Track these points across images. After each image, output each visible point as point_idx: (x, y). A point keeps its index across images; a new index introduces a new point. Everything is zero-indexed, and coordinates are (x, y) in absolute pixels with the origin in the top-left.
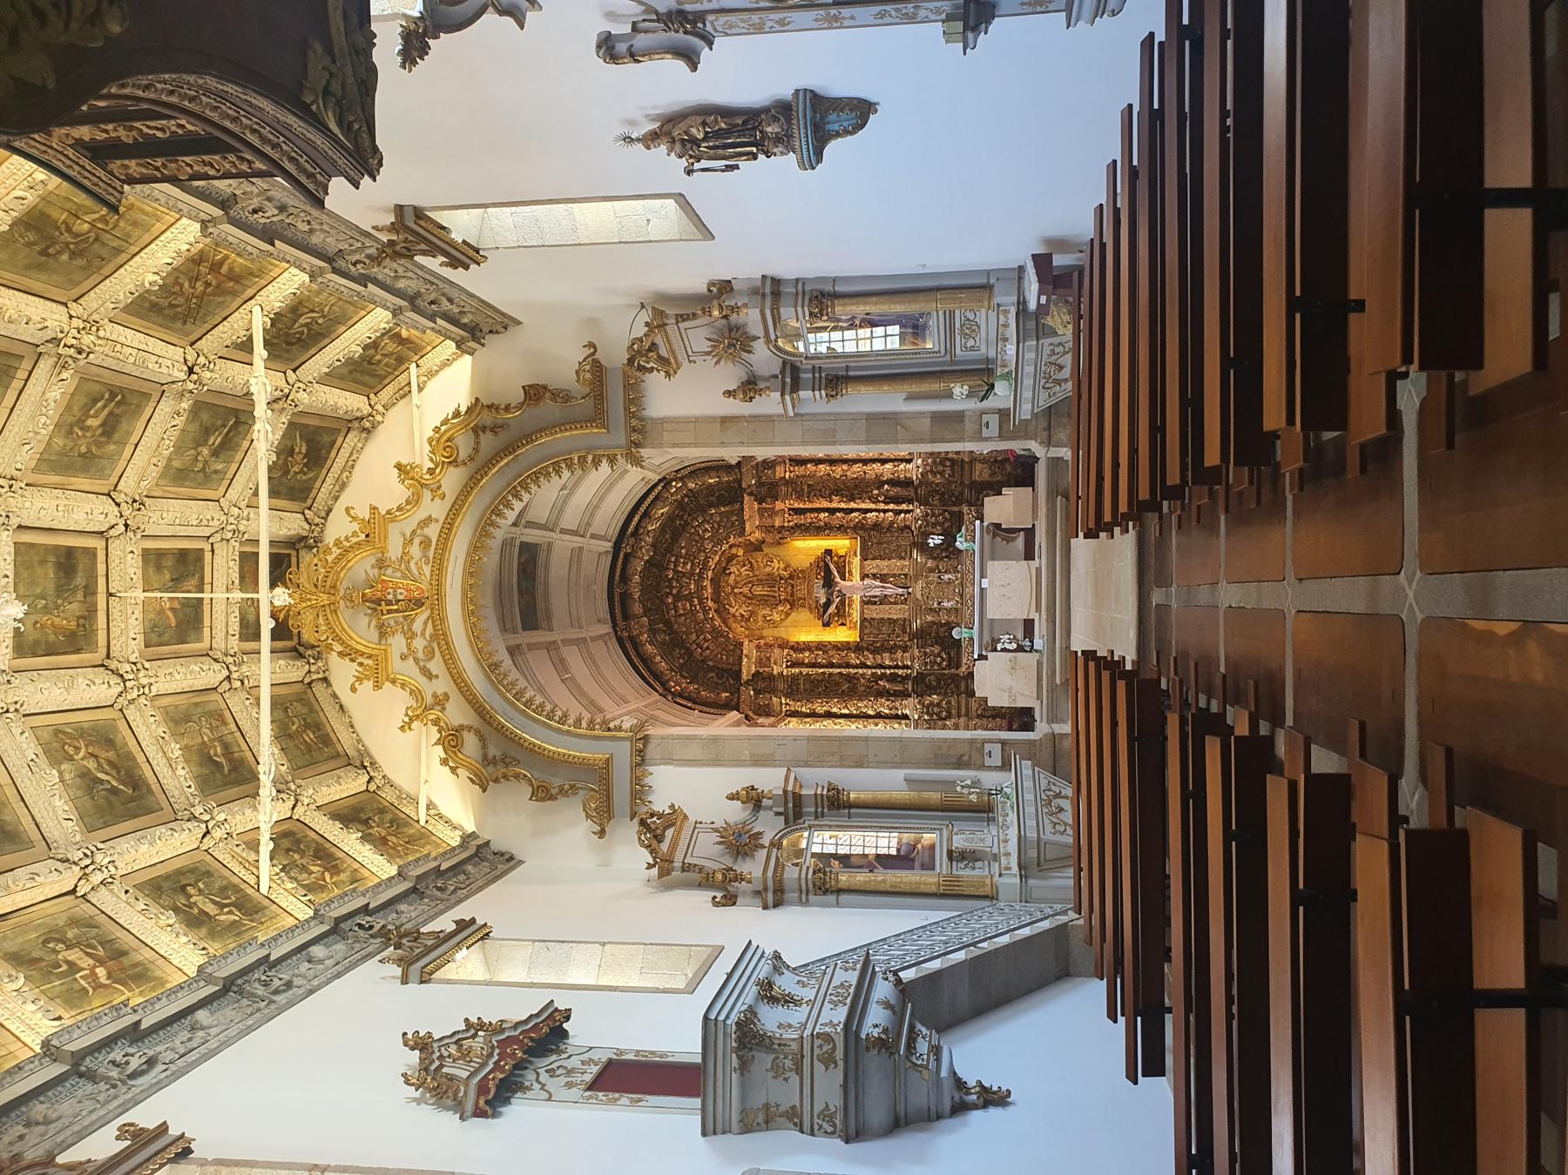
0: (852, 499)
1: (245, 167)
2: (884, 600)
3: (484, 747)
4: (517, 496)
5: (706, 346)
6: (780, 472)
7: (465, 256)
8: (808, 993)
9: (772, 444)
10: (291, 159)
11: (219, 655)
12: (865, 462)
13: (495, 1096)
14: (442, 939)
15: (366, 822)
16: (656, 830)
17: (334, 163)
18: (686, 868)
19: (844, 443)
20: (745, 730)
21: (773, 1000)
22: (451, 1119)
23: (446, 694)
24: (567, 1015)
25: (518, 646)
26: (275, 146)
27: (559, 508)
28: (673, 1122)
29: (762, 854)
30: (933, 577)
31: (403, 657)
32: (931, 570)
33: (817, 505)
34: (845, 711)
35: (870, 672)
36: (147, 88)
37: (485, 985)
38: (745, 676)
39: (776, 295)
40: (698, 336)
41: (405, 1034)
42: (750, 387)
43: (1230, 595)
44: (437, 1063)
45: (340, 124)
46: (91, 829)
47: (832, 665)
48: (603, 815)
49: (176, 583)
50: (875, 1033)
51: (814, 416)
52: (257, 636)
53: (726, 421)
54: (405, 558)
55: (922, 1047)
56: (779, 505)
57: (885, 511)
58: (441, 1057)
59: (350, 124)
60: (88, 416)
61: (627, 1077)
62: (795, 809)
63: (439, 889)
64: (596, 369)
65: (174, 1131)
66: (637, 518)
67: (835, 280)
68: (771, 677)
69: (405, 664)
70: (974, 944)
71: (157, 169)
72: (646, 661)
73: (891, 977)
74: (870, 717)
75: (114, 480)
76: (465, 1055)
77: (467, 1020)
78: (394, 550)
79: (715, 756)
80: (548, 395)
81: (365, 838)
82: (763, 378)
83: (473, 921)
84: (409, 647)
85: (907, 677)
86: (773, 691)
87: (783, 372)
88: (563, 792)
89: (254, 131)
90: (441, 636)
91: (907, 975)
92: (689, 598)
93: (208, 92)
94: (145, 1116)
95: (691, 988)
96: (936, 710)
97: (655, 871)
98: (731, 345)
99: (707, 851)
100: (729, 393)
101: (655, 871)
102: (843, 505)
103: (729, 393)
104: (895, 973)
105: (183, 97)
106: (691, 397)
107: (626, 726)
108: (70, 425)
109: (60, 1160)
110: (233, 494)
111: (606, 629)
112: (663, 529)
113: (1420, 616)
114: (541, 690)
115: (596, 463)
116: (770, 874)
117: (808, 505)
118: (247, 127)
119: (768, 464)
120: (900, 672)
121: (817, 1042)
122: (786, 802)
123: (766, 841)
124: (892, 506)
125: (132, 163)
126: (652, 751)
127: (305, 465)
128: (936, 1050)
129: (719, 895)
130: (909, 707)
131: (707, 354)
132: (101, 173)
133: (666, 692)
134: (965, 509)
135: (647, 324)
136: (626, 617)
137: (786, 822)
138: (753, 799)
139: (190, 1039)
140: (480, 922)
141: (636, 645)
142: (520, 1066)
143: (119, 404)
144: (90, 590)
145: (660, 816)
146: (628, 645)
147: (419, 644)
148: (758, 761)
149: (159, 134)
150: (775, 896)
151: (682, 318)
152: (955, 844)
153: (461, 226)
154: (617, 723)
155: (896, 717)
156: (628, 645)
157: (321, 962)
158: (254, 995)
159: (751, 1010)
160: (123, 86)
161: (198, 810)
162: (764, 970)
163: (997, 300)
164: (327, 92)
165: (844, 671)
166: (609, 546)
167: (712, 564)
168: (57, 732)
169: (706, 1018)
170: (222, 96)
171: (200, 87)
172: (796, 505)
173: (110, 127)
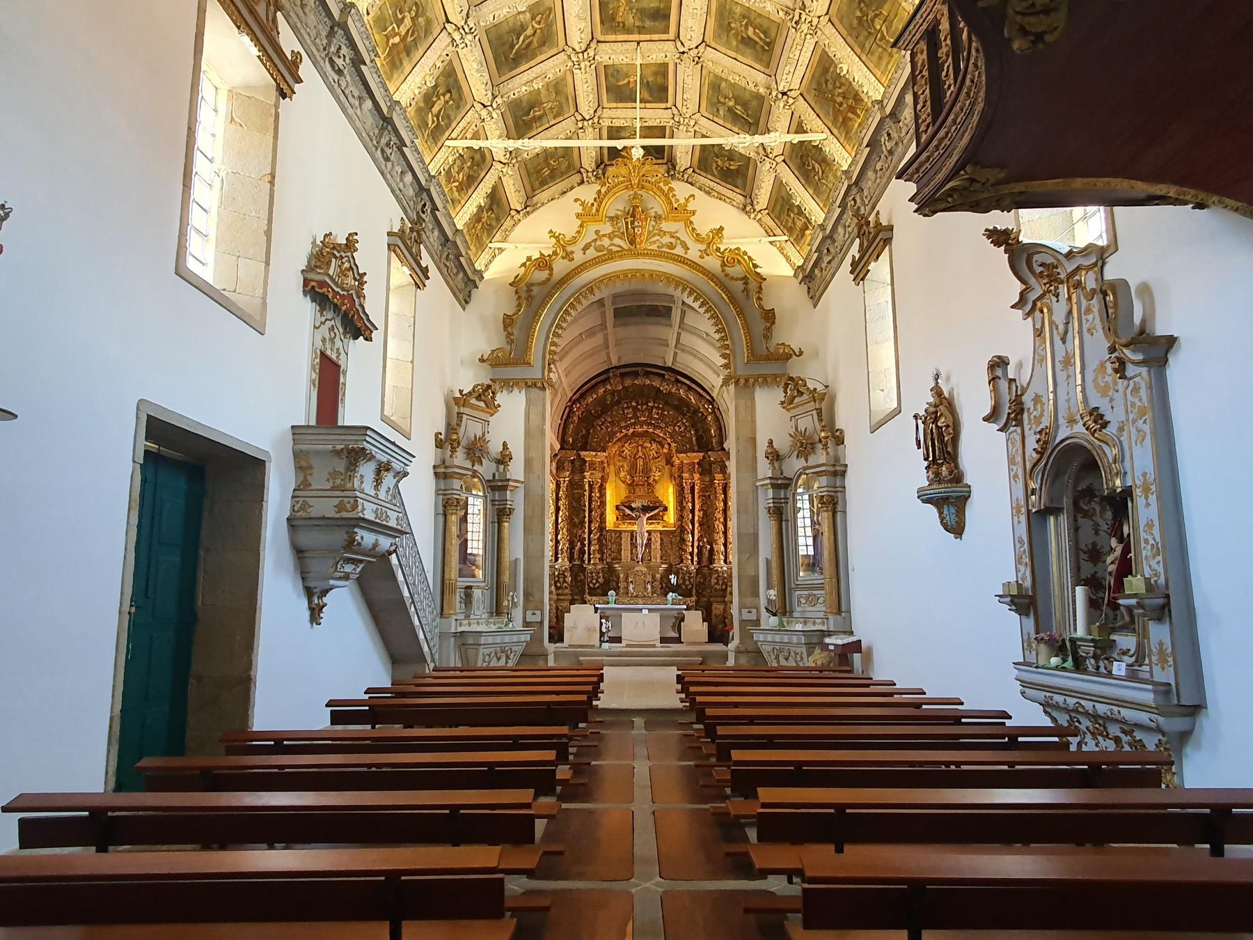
0: (701, 525)
1: (923, 128)
2: (634, 545)
5: (801, 427)
6: (719, 476)
7: (859, 271)
8: (382, 495)
9: (738, 471)
10: (928, 158)
12: (725, 533)
13: (317, 292)
15: (491, 209)
16: (484, 395)
26: (937, 147)
27: (694, 331)
30: (649, 578)
31: (597, 232)
32: (653, 577)
37: (387, 286)
38: (583, 453)
40: (808, 423)
42: (775, 456)
43: (642, 768)
45: (952, 189)
47: (590, 512)
48: (493, 361)
49: (646, 85)
50: (358, 538)
53: (753, 440)
54: (662, 233)
55: (348, 568)
56: (697, 476)
58: (342, 257)
59: (951, 196)
61: (329, 377)
64: (786, 356)
65: (297, 87)
67: (844, 512)
70: (413, 602)
73: (393, 548)
75: (713, 45)
79: (532, 435)
81: (480, 208)
83: (428, 278)
87: (785, 478)
89: (947, 134)
90: (611, 256)
91: (393, 558)
93: (973, 105)
94: (306, 69)
95: (384, 419)
99: (470, 429)
100: (771, 442)
103: (771, 442)
106: (769, 418)
107: (552, 375)
109: (279, 14)
110: (703, 121)
111: (615, 362)
112: (681, 399)
113: (633, 891)
115: (724, 356)
117: (696, 496)
119: (723, 469)
121: (352, 500)
125: (925, 56)
126: (535, 392)
128: (346, 577)
129: (442, 437)
130: (563, 562)
133: (573, 402)
134: (694, 599)
138: (504, 459)
140: (427, 282)
141: (603, 381)
142: (336, 308)
144: (641, 30)
145: (493, 398)
147: (606, 242)
148: (528, 463)
149: (944, 74)
150: (442, 473)
153: (879, 269)
157: (402, 180)
162: (397, 466)
164: (972, 181)
170: (970, 113)
173: (948, 42)
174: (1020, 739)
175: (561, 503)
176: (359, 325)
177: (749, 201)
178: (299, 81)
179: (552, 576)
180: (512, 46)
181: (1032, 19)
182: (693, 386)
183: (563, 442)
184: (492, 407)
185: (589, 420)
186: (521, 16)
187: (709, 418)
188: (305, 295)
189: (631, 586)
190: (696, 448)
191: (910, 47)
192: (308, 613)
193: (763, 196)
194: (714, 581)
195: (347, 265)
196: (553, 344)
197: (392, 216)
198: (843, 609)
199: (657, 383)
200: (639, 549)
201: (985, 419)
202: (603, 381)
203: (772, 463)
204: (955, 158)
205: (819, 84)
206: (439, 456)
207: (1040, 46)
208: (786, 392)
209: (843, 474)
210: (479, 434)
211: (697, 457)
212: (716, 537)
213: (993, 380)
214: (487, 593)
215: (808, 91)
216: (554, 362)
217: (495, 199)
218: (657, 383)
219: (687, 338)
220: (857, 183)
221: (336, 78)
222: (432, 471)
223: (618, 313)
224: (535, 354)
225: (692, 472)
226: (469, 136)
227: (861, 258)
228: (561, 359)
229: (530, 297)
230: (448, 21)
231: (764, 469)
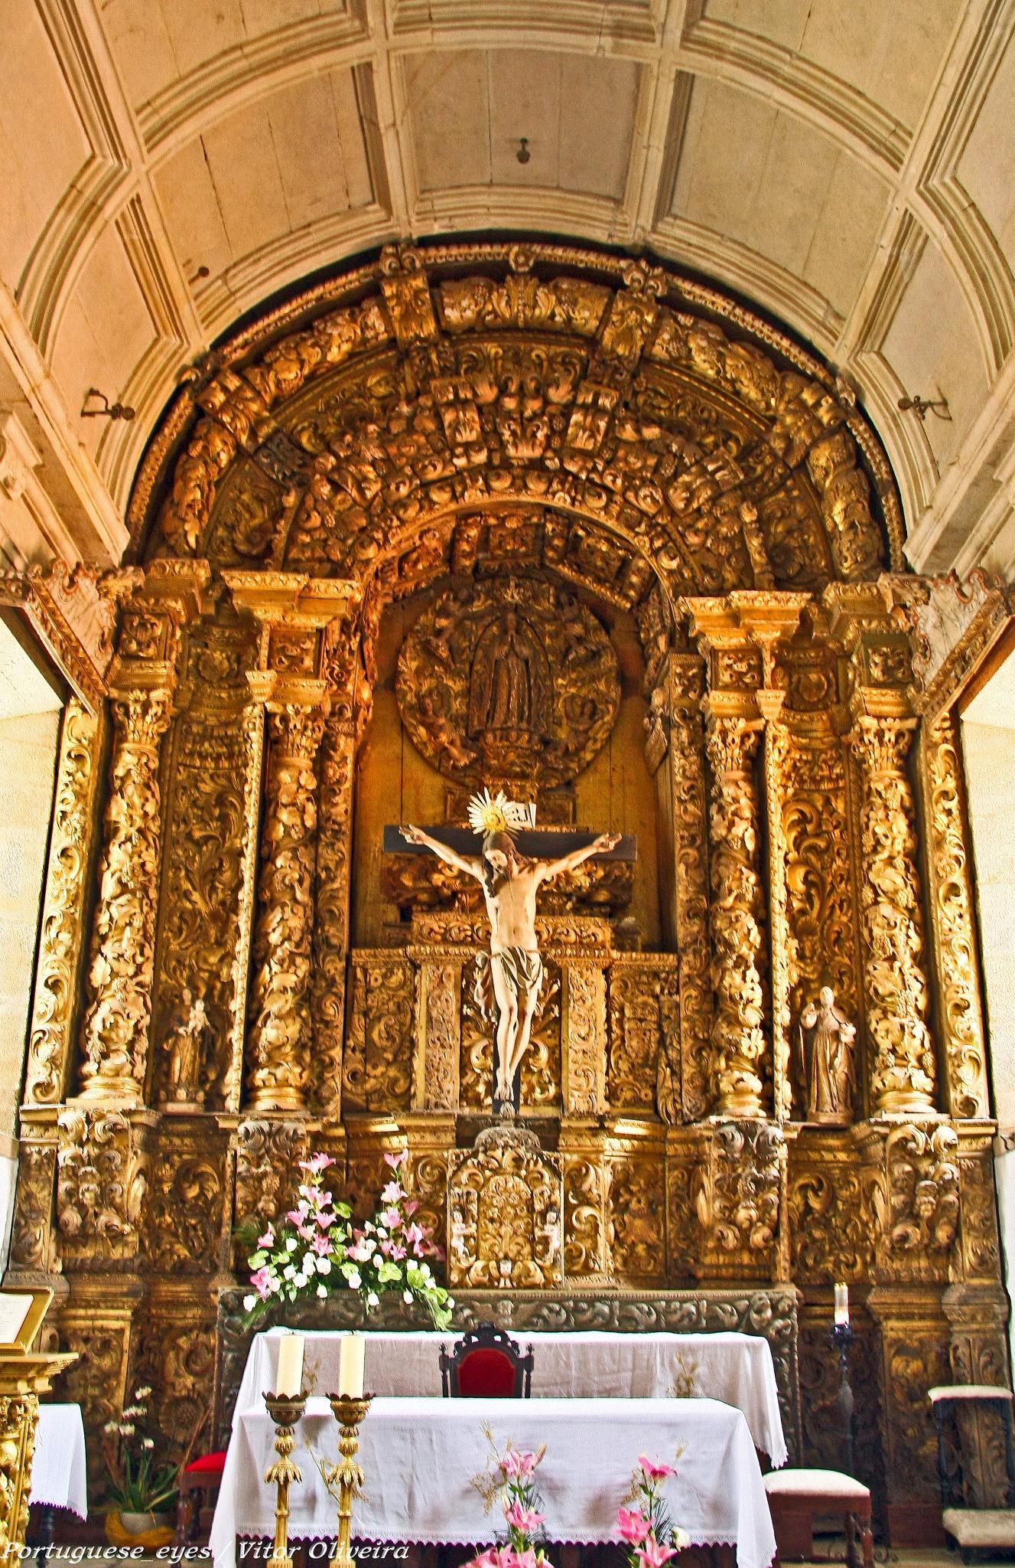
34: (109, 887)
35: (238, 973)
38: (237, 580)
96: (89, 1193)
141: (353, 303)
174: (936, 1394)
175: (118, 810)
185: (283, 461)
194: (884, 1201)
202: (353, 303)
212: (882, 979)
225: (748, 687)
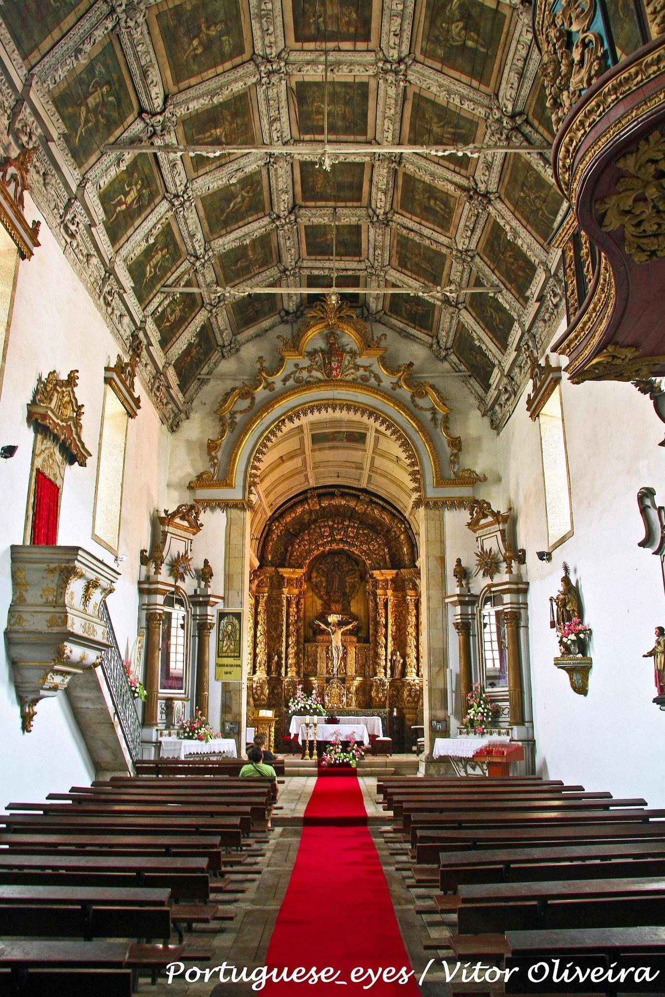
0: (394, 639)
1: (571, 310)
3: (241, 412)
4: (393, 433)
5: (487, 547)
6: (411, 593)
7: (535, 408)
8: (90, 609)
9: (428, 589)
10: (576, 337)
11: (299, 264)
12: (417, 647)
13: (37, 421)
14: (130, 388)
15: (199, 344)
16: (189, 514)
17: (576, 359)
18: (165, 534)
19: (429, 635)
20: (247, 570)
21: (87, 589)
22: (28, 399)
23: (274, 389)
24: (83, 464)
25: (302, 431)
26: (582, 329)
27: (384, 455)
28: (15, 529)
29: (171, 581)
31: (296, 365)
33: (390, 616)
36: (606, 269)
37: (100, 412)
38: (280, 570)
39: (518, 591)
40: (493, 543)
41: (77, 371)
42: (462, 574)
44: (60, 390)
45: (598, 363)
46: (203, 199)
47: (288, 626)
48: (200, 481)
49: (341, 243)
50: (67, 651)
51: (445, 615)
52: (310, 285)
53: (442, 560)
54: (357, 367)
55: (58, 679)
56: (390, 592)
57: (386, 659)
58: (63, 392)
59: (597, 369)
60: (436, 199)
61: (45, 500)
62: (200, 600)
63: (158, 387)
64: (473, 480)
65: (35, 250)
66: (381, 503)
67: (527, 627)
68: (280, 587)
69: (293, 366)
70: (116, 713)
71: (570, 266)
72: (292, 508)
73: (99, 661)
74: (255, 650)
75: (400, 211)
76: (62, 406)
77: (83, 406)
78: (361, 361)
79: (231, 552)
80: (455, 451)
81: (190, 345)
82: (468, 584)
83: (139, 408)
84: (304, 368)
85: (280, 674)
86: (271, 587)
87: (472, 595)
88: (212, 459)
89: (589, 319)
90: (308, 385)
91: (99, 670)
92: (331, 534)
93: (608, 298)
94: (45, 234)
95: (96, 538)
96: (259, 692)
97: (163, 515)
98: (487, 563)
99: (174, 547)
100: (459, 561)
101: (163, 515)
102: (390, 632)
103: (459, 561)
104: (101, 664)
105: (603, 286)
106: (456, 538)
107: (252, 497)
108: (431, 191)
109: (26, 193)
110: (392, 272)
111: (312, 483)
112: (374, 519)
114: (275, 446)
115: (415, 480)
116: (160, 586)
117: (389, 613)
118: (591, 315)
119: (415, 587)
120: (283, 669)
121: (62, 615)
122: (203, 596)
123: (179, 583)
124: (389, 664)
125: (571, 254)
126: (235, 513)
127: (410, 312)
128: (55, 688)
129: (147, 554)
130: (261, 675)
131: (482, 548)
132: (566, 238)
133: (273, 519)
134: (387, 710)
135: (499, 512)
136: (320, 496)
137: (191, 597)
138: (205, 574)
139: (82, 255)
140: (138, 411)
141: (301, 502)
142: (56, 438)
143: (443, 216)
144: (337, 199)
145: (196, 518)
146: (301, 497)
147: (305, 374)
148: (228, 578)
149: (585, 269)
150: (146, 588)
151: (503, 532)
152: (176, 702)
153: (552, 406)
154: (254, 491)
155: (254, 667)
156: (301, 497)
157: (120, 322)
158: (103, 287)
159: (82, 576)
160: (605, 259)
161: (211, 254)
162: (104, 583)
163: (515, 728)
164: (614, 357)
165: (284, 633)
166: (364, 484)
167: (353, 549)
168: (259, 183)
169: (78, 548)
170: (606, 305)
171: (609, 295)
172: (389, 603)
173: (588, 245)
174: (651, 820)
176: (75, 452)
177: (435, 341)
178: (38, 244)
179: (250, 688)
180: (222, 212)
181: (645, 241)
182: (387, 506)
183: (262, 557)
184: (196, 527)
186: (232, 188)
187: (402, 537)
188: (29, 426)
189: (326, 698)
190: (389, 565)
191: (562, 245)
192: (20, 721)
193: (446, 337)
195: (66, 399)
196: (256, 468)
197: (112, 350)
198: (527, 718)
199: (352, 504)
200: (335, 662)
201: (640, 545)
203: (460, 581)
204: (595, 341)
205: (492, 247)
206: (144, 573)
207: (654, 258)
208: (472, 514)
209: (525, 591)
210: (182, 552)
211: (390, 574)
213: (644, 511)
214: (188, 704)
215: (485, 250)
216: (254, 484)
217: (206, 334)
218: (352, 504)
219: (378, 461)
220: (529, 331)
221: (69, 240)
222: (136, 586)
223: (315, 439)
224: (238, 478)
226: (182, 283)
227: (535, 397)
228: (261, 481)
229: (233, 424)
230: (167, 191)
231: (453, 588)
